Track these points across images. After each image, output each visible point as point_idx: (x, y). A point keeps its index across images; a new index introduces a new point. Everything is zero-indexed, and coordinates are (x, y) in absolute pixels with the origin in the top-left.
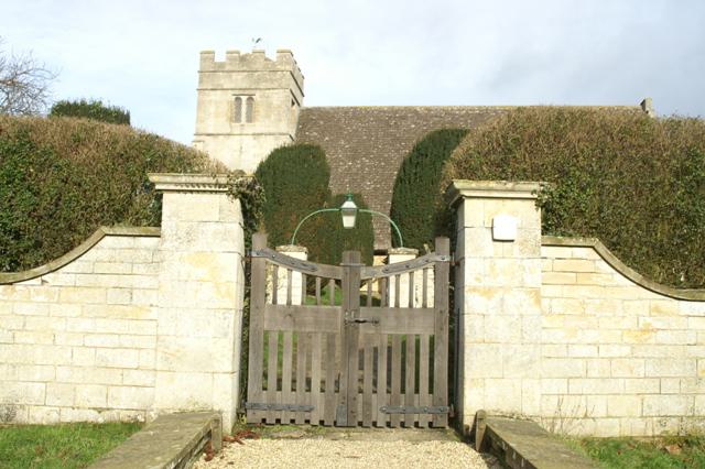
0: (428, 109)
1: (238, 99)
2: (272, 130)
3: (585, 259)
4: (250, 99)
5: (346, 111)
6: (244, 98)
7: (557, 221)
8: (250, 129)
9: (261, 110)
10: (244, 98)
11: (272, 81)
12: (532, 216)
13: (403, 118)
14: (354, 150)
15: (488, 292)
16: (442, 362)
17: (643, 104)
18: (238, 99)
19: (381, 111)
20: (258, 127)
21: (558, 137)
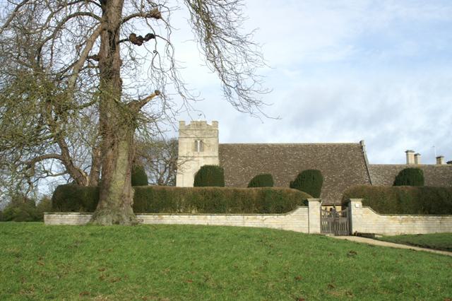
0: (273, 145)
1: (196, 142)
2: (211, 155)
3: (368, 209)
4: (201, 141)
5: (238, 145)
6: (199, 141)
7: (365, 204)
8: (202, 154)
9: (206, 148)
10: (199, 141)
11: (211, 134)
12: (361, 204)
13: (263, 149)
14: (244, 163)
15: (355, 215)
16: (348, 225)
17: (361, 142)
18: (196, 142)
19: (253, 145)
20: (206, 153)
21: (362, 190)
